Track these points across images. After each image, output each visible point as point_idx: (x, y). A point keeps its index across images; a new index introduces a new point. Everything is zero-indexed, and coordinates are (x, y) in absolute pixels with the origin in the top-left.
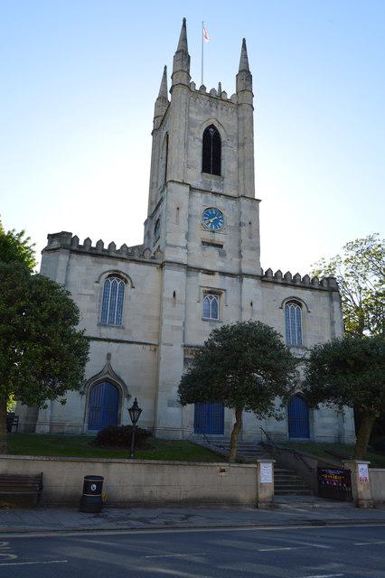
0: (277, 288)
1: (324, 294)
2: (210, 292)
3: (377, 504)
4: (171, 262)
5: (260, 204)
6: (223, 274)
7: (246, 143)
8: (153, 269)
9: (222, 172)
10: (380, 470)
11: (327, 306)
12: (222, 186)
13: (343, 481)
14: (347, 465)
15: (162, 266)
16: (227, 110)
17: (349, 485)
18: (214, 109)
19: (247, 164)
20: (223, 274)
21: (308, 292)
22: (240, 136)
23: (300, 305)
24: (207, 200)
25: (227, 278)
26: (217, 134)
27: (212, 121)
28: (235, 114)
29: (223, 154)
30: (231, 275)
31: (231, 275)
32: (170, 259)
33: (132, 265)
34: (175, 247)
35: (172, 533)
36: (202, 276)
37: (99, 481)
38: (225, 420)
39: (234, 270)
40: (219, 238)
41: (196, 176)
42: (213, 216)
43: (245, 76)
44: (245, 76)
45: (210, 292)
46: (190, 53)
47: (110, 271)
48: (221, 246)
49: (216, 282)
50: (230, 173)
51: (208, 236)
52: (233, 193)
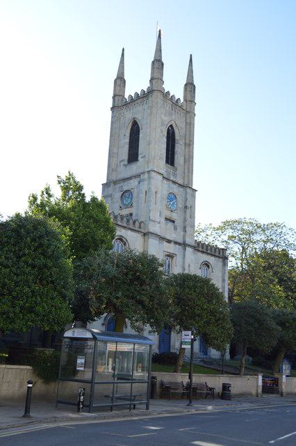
0: (200, 254)
1: (221, 260)
2: (168, 256)
3: (290, 394)
4: (184, 255)
5: (197, 192)
6: (176, 243)
7: (189, 144)
9: (176, 164)
10: (9, 366)
11: (221, 268)
12: (175, 175)
13: (274, 384)
14: (276, 376)
15: (145, 234)
17: (277, 385)
18: (173, 112)
19: (189, 159)
20: (176, 243)
21: (213, 258)
22: (187, 137)
23: (208, 267)
24: (169, 187)
25: (177, 246)
27: (172, 123)
28: (184, 119)
30: (179, 244)
31: (179, 244)
32: (151, 230)
33: (129, 232)
34: (154, 221)
35: (124, 421)
36: (165, 244)
37: (229, 386)
38: (171, 344)
39: (180, 240)
40: (174, 216)
41: (161, 165)
42: (172, 197)
43: (190, 87)
44: (190, 87)
45: (168, 256)
46: (163, 60)
48: (173, 222)
50: (180, 165)
52: (181, 182)
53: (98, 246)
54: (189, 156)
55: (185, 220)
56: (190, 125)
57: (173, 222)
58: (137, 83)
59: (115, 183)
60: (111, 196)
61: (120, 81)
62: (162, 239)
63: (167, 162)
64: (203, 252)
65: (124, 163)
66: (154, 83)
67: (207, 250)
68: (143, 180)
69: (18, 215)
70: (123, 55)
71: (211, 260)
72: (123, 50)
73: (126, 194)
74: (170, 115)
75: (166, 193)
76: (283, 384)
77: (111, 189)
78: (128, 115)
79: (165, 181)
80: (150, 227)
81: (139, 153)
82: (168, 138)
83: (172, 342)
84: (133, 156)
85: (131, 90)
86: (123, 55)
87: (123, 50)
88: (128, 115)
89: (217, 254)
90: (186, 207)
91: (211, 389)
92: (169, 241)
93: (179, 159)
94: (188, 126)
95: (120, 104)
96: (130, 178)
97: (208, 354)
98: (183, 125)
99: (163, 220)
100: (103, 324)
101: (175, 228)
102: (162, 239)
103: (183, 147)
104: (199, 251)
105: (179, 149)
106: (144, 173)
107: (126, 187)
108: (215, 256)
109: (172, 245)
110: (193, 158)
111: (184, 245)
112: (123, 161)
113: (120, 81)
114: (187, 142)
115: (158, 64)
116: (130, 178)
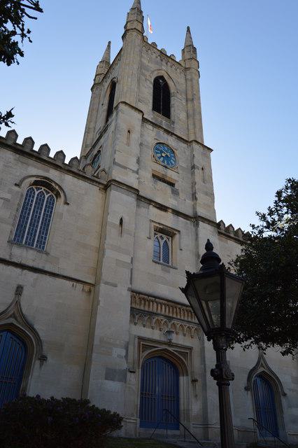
4: (197, 235)
8: (94, 190)
26: (166, 86)
28: (183, 75)
29: (172, 102)
30: (186, 216)
34: (125, 168)
38: (182, 407)
39: (189, 212)
44: (190, 49)
47: (38, 176)
49: (168, 220)
51: (160, 170)
53: (276, 206)
54: (194, 110)
57: (172, 185)
80: (113, 173)
83: (182, 401)
90: (193, 167)
91: (237, 261)
92: (163, 208)
94: (189, 83)
95: (105, 61)
97: (281, 432)
103: (184, 102)
104: (230, 237)
105: (177, 104)
109: (170, 215)
110: (200, 113)
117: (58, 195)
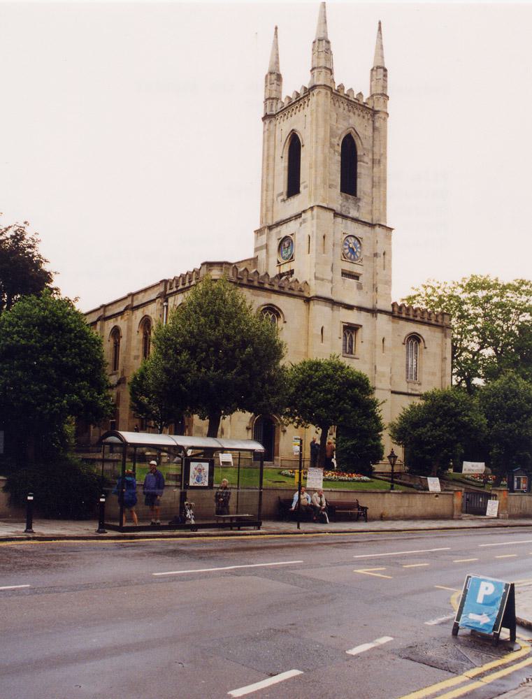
0: (402, 323)
7: (378, 161)
15: (308, 300)
16: (364, 117)
19: (379, 183)
20: (360, 309)
28: (371, 122)
36: (343, 311)
39: (369, 305)
43: (380, 71)
44: (380, 71)
49: (353, 317)
51: (348, 267)
55: (375, 274)
56: (378, 131)
58: (295, 79)
59: (270, 228)
60: (267, 246)
61: (275, 77)
62: (333, 303)
63: (344, 189)
64: (408, 320)
65: (281, 198)
66: (315, 74)
67: (400, 313)
68: (304, 221)
69: (46, 277)
70: (380, 29)
71: (423, 331)
72: (380, 23)
73: (286, 243)
74: (346, 119)
75: (340, 237)
76: (194, 427)
77: (264, 237)
78: (284, 128)
79: (339, 220)
81: (301, 181)
82: (343, 155)
84: (293, 188)
85: (289, 89)
86: (380, 29)
87: (380, 23)
88: (284, 128)
89: (433, 322)
93: (363, 184)
96: (289, 220)
98: (369, 132)
99: (338, 276)
100: (248, 429)
101: (360, 287)
102: (333, 303)
105: (363, 169)
106: (304, 211)
107: (285, 231)
108: (429, 324)
111: (374, 312)
112: (282, 194)
113: (275, 77)
114: (376, 157)
115: (323, 45)
116: (289, 220)
117: (278, 316)
